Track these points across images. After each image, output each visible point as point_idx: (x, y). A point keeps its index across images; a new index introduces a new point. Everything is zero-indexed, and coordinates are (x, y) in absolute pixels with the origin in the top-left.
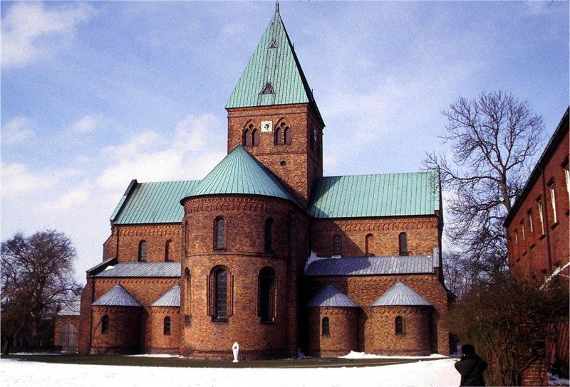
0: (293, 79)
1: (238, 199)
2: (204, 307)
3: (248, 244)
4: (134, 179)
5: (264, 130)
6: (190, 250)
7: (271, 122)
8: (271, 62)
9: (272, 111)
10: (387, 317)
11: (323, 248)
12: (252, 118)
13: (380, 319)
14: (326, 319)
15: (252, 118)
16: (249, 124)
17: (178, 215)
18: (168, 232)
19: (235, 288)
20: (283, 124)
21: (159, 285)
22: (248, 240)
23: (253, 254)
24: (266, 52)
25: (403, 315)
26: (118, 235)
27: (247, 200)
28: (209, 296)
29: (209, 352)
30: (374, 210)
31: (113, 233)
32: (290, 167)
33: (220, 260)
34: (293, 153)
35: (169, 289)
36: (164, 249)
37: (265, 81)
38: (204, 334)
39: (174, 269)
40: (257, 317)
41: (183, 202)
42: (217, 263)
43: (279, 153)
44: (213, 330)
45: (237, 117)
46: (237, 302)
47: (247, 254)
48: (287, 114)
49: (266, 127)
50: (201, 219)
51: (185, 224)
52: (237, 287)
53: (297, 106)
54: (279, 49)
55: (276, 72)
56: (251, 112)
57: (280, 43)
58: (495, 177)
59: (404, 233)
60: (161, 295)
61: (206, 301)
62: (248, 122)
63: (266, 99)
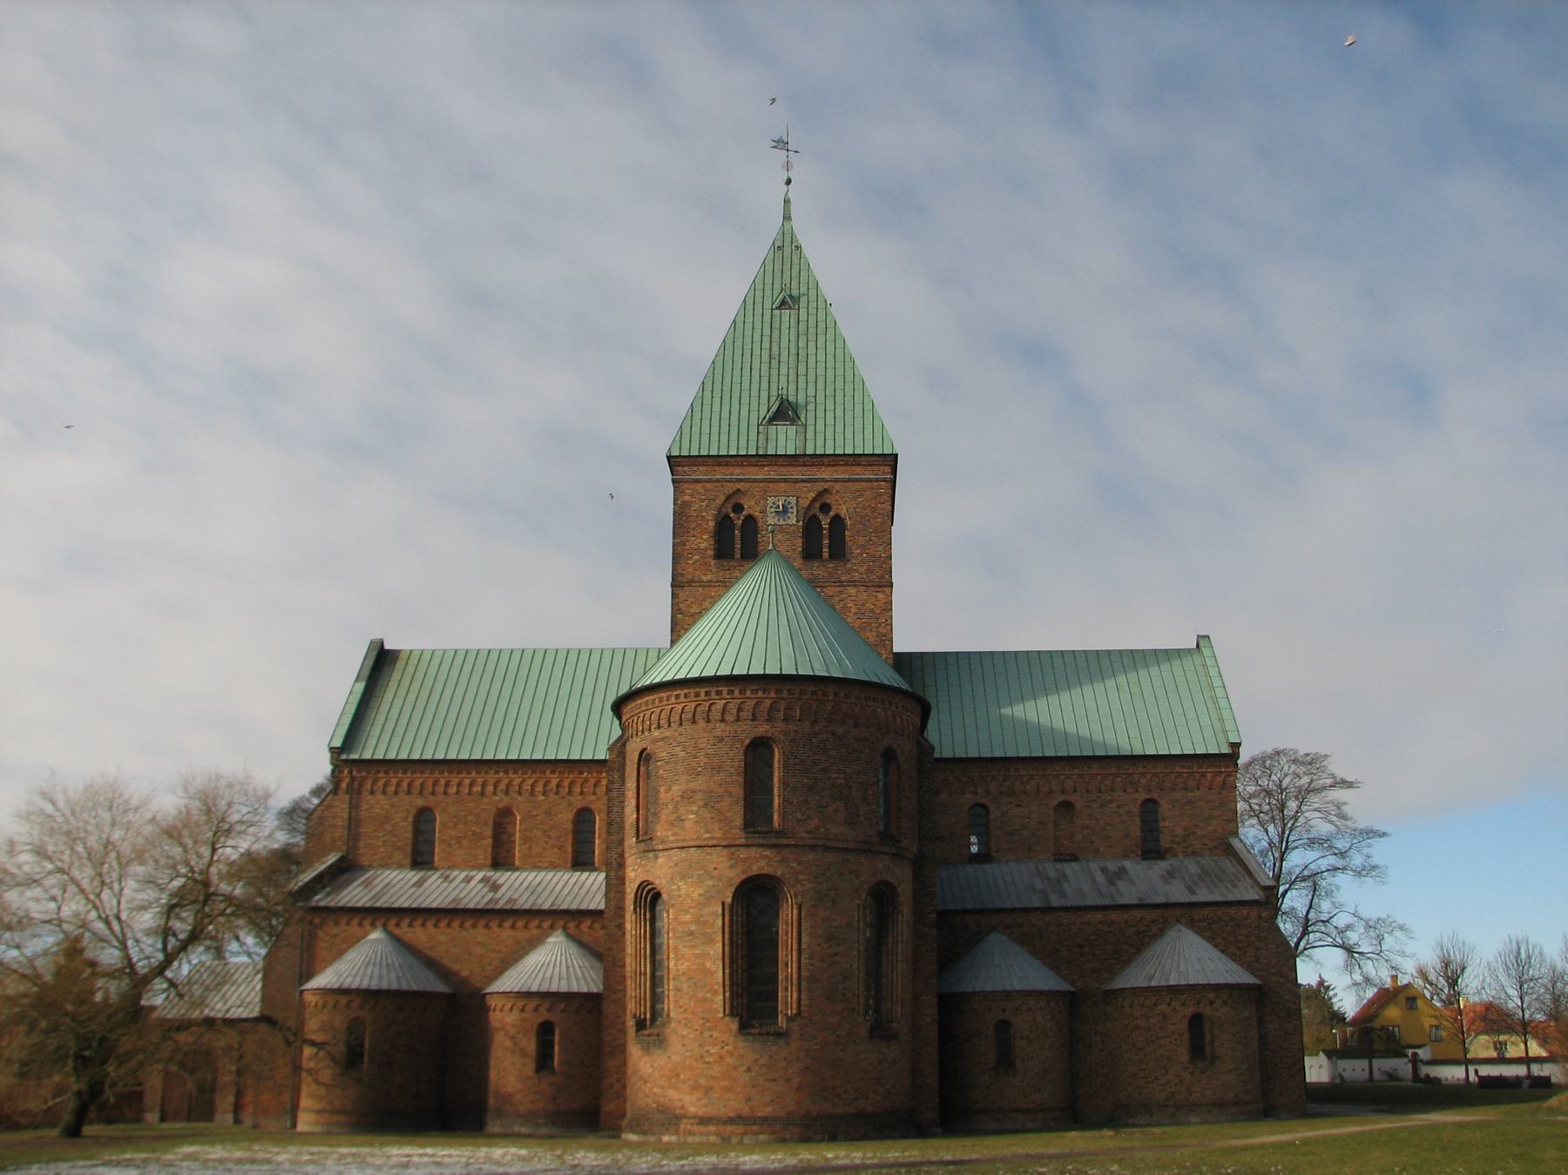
1: (814, 693)
2: (715, 993)
5: (772, 520)
7: (793, 500)
9: (797, 473)
10: (1165, 1016)
14: (1003, 1025)
16: (733, 501)
18: (502, 786)
19: (805, 939)
21: (506, 934)
23: (851, 845)
24: (767, 318)
25: (1208, 1011)
27: (836, 695)
34: (853, 583)
36: (488, 832)
37: (774, 393)
42: (755, 870)
44: (741, 1057)
45: (698, 481)
47: (835, 844)
48: (836, 480)
49: (778, 512)
50: (702, 743)
53: (864, 461)
55: (802, 371)
56: (737, 470)
59: (1152, 801)
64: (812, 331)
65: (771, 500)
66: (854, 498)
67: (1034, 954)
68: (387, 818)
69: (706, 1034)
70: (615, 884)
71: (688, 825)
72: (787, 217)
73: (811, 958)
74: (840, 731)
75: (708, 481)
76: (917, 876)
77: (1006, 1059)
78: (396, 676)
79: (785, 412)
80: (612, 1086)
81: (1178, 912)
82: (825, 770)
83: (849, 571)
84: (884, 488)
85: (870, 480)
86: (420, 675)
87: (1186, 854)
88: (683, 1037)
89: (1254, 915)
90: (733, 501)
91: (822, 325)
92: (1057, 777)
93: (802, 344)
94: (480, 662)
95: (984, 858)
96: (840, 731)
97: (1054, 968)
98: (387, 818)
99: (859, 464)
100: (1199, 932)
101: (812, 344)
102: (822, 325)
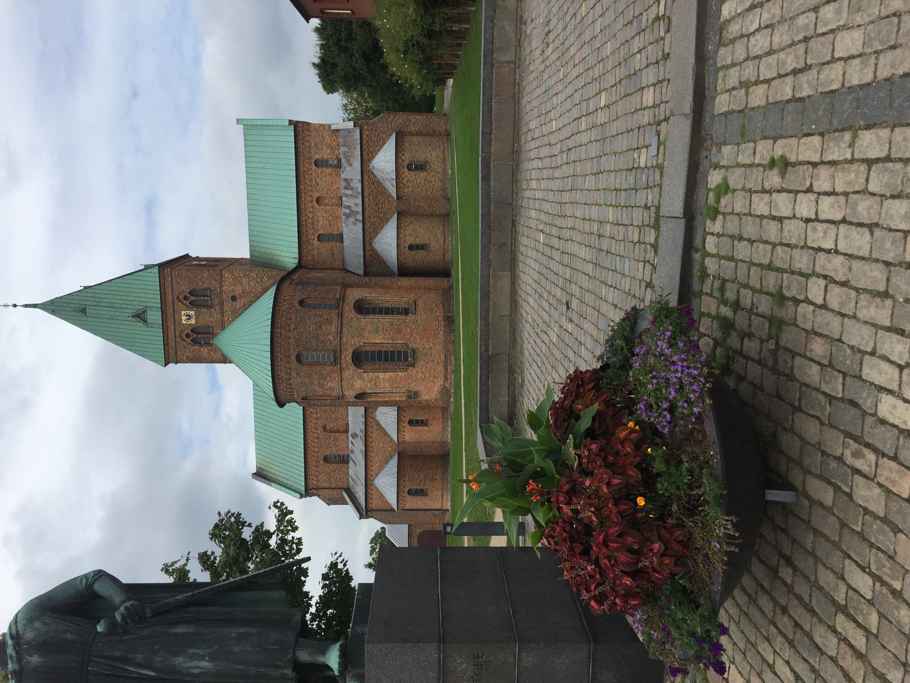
0: (128, 285)
3: (329, 327)
4: (251, 476)
5: (193, 321)
6: (335, 393)
7: (183, 312)
8: (104, 313)
9: (170, 311)
11: (333, 255)
13: (410, 189)
14: (411, 247)
17: (294, 411)
21: (375, 434)
24: (91, 319)
25: (406, 163)
26: (317, 489)
28: (385, 370)
29: (446, 369)
30: (291, 250)
31: (315, 495)
32: (238, 290)
33: (347, 357)
34: (221, 287)
35: (378, 424)
37: (131, 319)
38: (427, 374)
39: (355, 417)
41: (281, 405)
42: (350, 361)
43: (221, 305)
46: (393, 339)
49: (188, 318)
50: (299, 381)
51: (306, 402)
52: (376, 338)
54: (86, 303)
55: (118, 306)
56: (170, 336)
60: (386, 434)
63: (153, 317)
65: (184, 322)
67: (382, 228)
68: (328, 474)
71: (332, 385)
72: (35, 306)
74: (293, 326)
77: (422, 247)
78: (267, 468)
79: (141, 316)
81: (365, 166)
83: (216, 289)
86: (268, 460)
87: (339, 149)
89: (366, 132)
94: (261, 435)
96: (293, 326)
97: (388, 220)
98: (328, 474)
100: (373, 157)
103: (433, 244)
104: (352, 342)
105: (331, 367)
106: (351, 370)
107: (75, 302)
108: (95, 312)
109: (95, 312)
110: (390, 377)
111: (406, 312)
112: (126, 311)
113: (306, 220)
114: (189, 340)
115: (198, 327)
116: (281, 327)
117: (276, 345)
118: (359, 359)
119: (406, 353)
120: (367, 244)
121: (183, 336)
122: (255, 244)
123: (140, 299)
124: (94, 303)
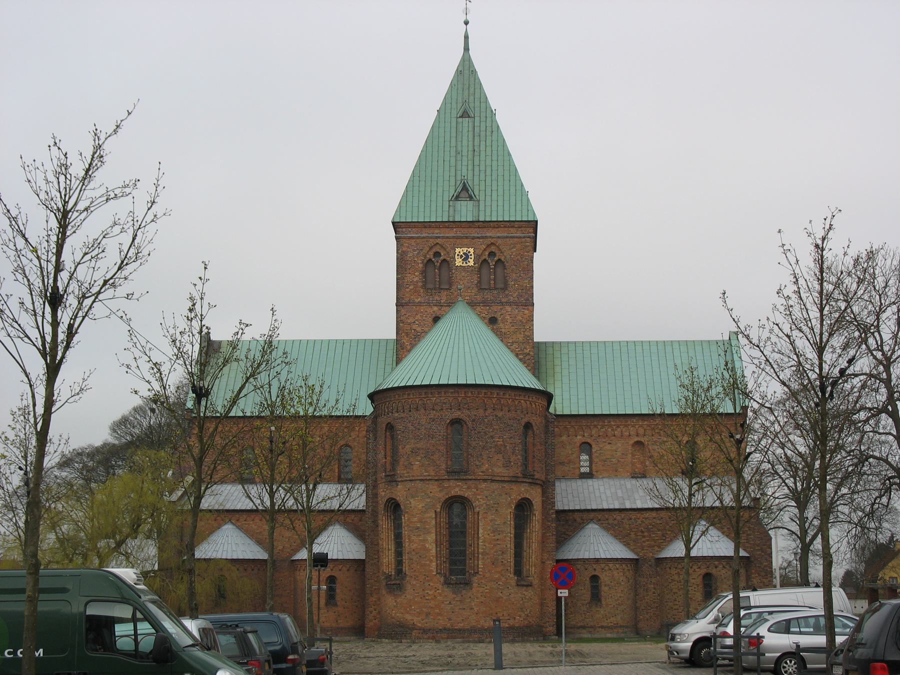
1: (485, 393)
5: (459, 262)
7: (472, 250)
8: (465, 143)
9: (474, 232)
11: (562, 463)
12: (439, 241)
13: (676, 577)
14: (595, 578)
15: (439, 241)
17: (366, 408)
20: (492, 254)
22: (500, 456)
24: (454, 124)
25: (714, 571)
28: (438, 543)
33: (457, 489)
34: (509, 303)
37: (459, 178)
38: (432, 604)
40: (512, 576)
42: (453, 493)
48: (499, 237)
49: (464, 257)
50: (423, 422)
53: (516, 225)
54: (477, 119)
55: (477, 162)
56: (437, 231)
57: (477, 109)
58: (824, 359)
61: (434, 551)
62: (431, 248)
63: (464, 209)
64: (483, 134)
65: (457, 250)
66: (510, 249)
69: (427, 584)
70: (372, 497)
71: (415, 467)
72: (466, 49)
73: (484, 542)
74: (500, 414)
75: (418, 238)
76: (544, 493)
77: (596, 596)
80: (371, 612)
82: (492, 437)
84: (529, 243)
85: (520, 237)
88: (414, 585)
90: (434, 250)
91: (489, 129)
92: (633, 426)
93: (476, 143)
95: (589, 476)
96: (500, 414)
97: (627, 544)
99: (513, 227)
101: (483, 143)
102: (489, 129)
103: (602, 611)
104: (481, 496)
105: (444, 466)
106: (440, 495)
107: (477, 104)
108: (465, 130)
109: (465, 130)
110: (429, 550)
111: (518, 572)
112: (470, 173)
113: (611, 426)
114: (430, 255)
115: (450, 270)
116: (498, 399)
117: (476, 391)
118: (456, 505)
119: (463, 572)
120: (592, 515)
121: (437, 249)
122: (564, 350)
123: (488, 193)
124: (477, 129)
